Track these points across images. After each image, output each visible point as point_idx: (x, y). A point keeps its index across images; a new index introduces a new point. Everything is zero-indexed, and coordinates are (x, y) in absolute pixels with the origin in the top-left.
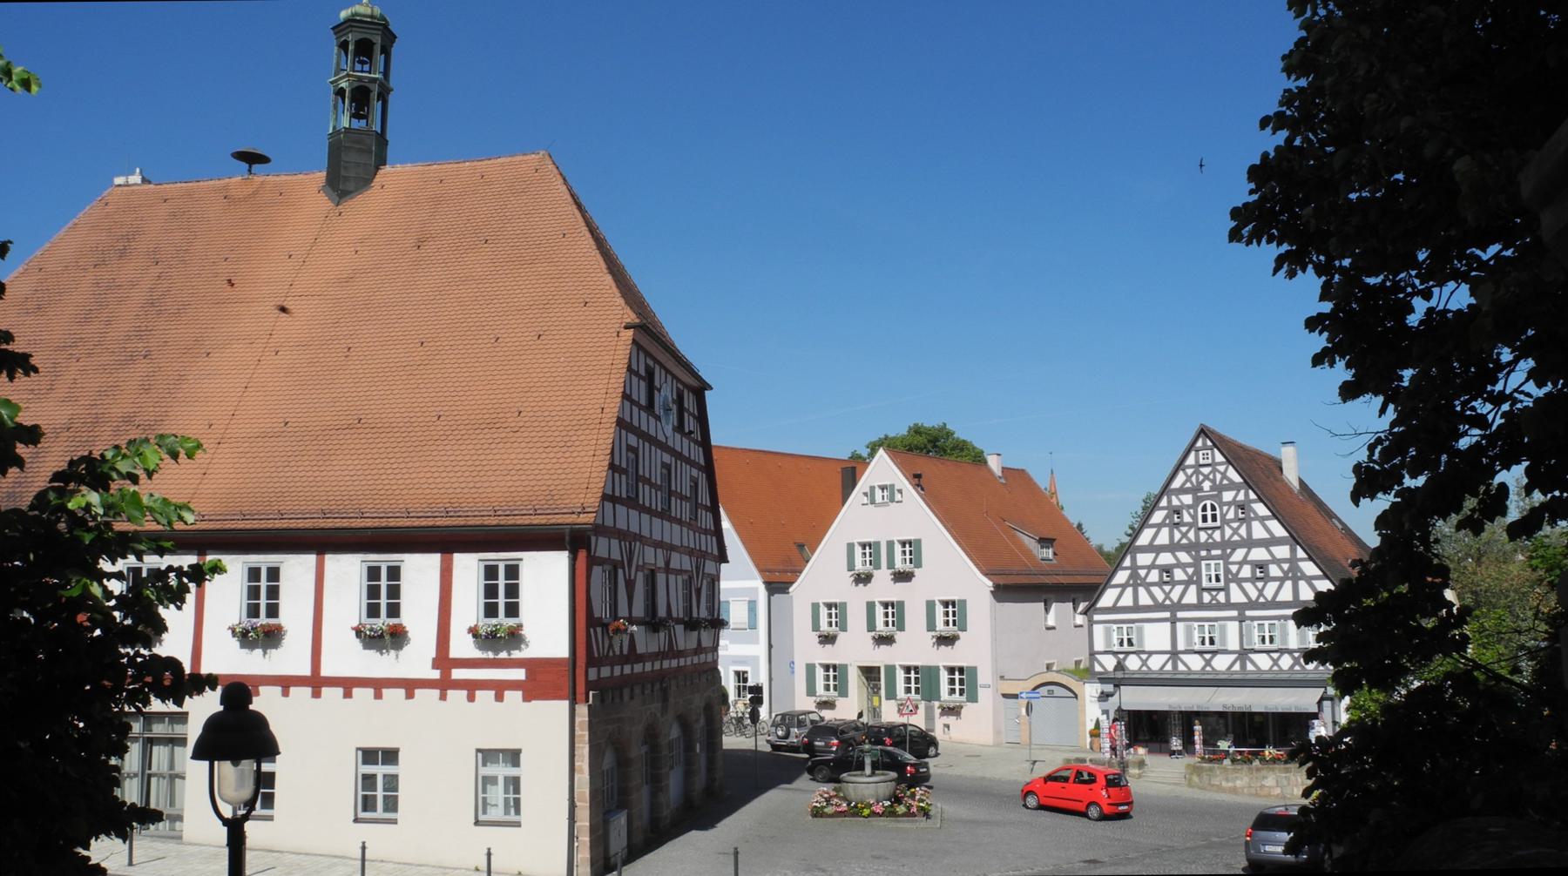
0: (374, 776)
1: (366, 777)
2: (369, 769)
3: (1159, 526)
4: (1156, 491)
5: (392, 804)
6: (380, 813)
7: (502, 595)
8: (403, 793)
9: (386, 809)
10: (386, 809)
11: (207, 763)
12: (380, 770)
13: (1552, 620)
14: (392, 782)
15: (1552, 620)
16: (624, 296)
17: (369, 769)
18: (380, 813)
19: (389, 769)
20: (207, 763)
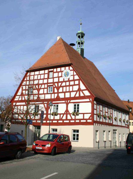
0: (75, 134)
1: (74, 134)
2: (74, 133)
3: (26, 81)
4: (13, 95)
5: (77, 139)
6: (76, 140)
7: (26, 87)
8: (79, 137)
9: (77, 140)
10: (77, 140)
11: (91, 112)
12: (76, 133)
13: (105, 125)
14: (78, 135)
15: (105, 125)
16: (46, 155)
17: (74, 133)
18: (76, 140)
19: (77, 133)
20: (91, 112)
